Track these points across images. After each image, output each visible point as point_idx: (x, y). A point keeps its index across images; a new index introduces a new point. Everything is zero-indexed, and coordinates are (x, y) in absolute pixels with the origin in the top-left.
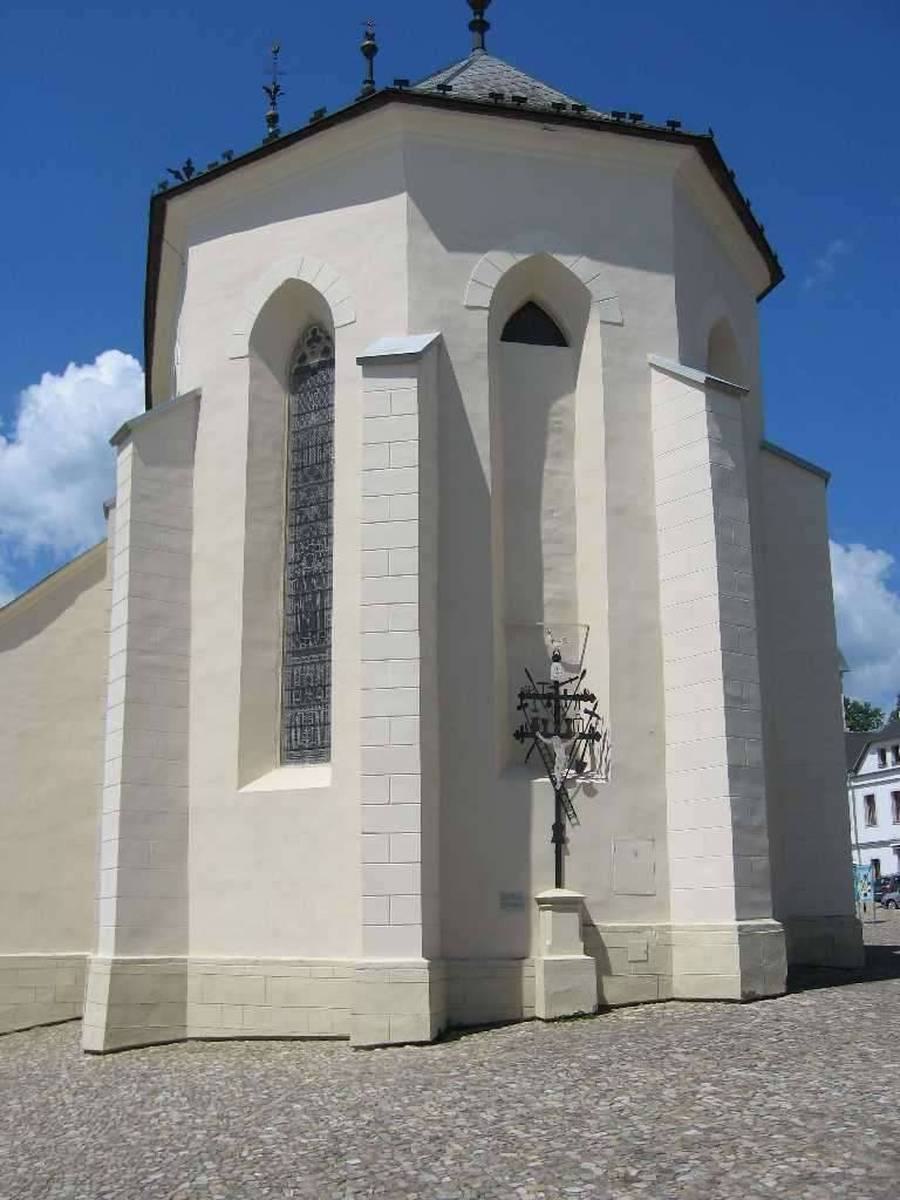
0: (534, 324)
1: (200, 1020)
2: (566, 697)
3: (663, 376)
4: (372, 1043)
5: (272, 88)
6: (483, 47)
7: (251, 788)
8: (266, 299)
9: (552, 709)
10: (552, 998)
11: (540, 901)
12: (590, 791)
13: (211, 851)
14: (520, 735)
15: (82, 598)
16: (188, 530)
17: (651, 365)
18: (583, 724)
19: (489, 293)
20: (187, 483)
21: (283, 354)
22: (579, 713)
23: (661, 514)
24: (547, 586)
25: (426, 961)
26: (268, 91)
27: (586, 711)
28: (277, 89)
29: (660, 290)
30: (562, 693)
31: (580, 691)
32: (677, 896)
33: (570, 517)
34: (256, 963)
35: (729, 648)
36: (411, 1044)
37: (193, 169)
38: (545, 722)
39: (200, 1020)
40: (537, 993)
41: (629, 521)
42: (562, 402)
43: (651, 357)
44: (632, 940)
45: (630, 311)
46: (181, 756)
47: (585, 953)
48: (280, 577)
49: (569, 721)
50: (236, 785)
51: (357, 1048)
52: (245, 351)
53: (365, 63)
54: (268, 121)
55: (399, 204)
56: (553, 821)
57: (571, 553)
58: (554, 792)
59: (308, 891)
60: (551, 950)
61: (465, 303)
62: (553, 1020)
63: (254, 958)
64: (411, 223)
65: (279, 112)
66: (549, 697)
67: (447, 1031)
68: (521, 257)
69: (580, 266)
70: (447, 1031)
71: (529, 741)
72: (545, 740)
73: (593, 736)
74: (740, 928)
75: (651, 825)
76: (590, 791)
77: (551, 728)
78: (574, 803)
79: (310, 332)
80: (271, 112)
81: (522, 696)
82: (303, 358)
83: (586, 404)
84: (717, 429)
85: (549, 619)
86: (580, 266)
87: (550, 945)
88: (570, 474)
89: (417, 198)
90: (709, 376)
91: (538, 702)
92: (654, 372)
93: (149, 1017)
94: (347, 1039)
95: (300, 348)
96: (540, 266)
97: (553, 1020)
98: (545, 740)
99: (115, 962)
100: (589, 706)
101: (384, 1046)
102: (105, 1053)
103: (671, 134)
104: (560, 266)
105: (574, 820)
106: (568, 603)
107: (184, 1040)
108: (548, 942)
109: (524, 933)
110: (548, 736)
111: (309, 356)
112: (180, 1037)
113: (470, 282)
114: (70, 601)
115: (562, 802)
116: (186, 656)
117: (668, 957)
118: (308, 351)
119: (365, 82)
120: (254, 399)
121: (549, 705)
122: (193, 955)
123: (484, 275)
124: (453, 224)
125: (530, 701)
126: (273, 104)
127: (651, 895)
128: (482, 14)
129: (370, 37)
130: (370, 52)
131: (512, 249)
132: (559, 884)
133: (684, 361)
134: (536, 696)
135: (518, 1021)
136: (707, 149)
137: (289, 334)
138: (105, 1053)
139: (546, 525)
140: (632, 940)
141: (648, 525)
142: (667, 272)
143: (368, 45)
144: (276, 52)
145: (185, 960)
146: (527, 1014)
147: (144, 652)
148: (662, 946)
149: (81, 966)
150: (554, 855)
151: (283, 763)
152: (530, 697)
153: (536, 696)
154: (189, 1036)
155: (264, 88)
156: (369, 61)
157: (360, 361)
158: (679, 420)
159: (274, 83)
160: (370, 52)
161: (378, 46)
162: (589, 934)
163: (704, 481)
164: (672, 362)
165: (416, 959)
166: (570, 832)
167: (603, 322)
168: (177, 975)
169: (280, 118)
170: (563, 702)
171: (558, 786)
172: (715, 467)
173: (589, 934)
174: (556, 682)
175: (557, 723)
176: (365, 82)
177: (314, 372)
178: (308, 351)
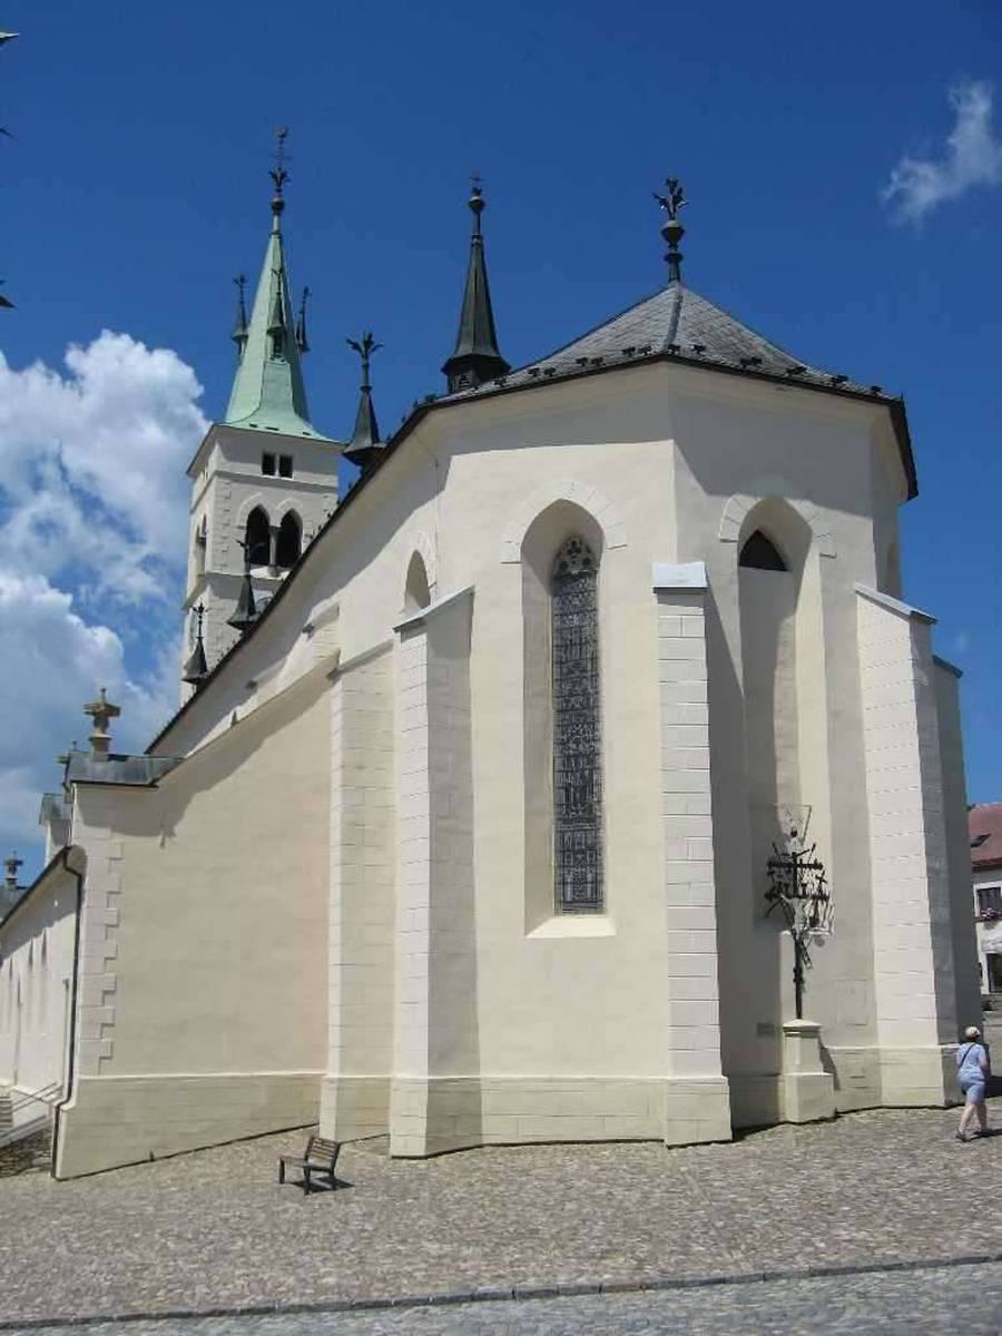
0: (764, 553)
1: (495, 1129)
2: (803, 866)
3: (867, 603)
4: (686, 1142)
5: (279, 176)
6: (679, 279)
7: (535, 934)
8: (536, 514)
9: (791, 876)
10: (805, 1105)
11: (787, 1029)
12: (820, 942)
13: (496, 988)
14: (769, 896)
15: (268, 742)
16: (467, 712)
17: (857, 592)
18: (812, 889)
19: (737, 529)
20: (466, 670)
21: (546, 557)
22: (808, 877)
23: (868, 720)
24: (778, 774)
25: (726, 1078)
26: (274, 176)
27: (817, 877)
28: (283, 176)
29: (863, 528)
30: (798, 862)
31: (812, 862)
32: (883, 1028)
33: (793, 717)
34: (550, 1080)
35: (929, 830)
36: (716, 1142)
37: (372, 343)
38: (787, 886)
39: (495, 1129)
40: (790, 1103)
41: (844, 724)
42: (788, 621)
43: (857, 586)
44: (852, 1061)
45: (837, 544)
46: (470, 906)
47: (825, 1071)
48: (550, 751)
49: (804, 885)
50: (523, 931)
51: (670, 1148)
52: (518, 557)
53: (471, 215)
54: (273, 208)
55: (668, 447)
56: (794, 965)
57: (794, 746)
58: (793, 941)
59: (607, 1017)
60: (800, 1068)
61: (720, 536)
62: (804, 1124)
63: (547, 1076)
64: (677, 465)
65: (285, 199)
66: (789, 865)
67: (740, 1132)
68: (759, 500)
69: (803, 508)
70: (740, 1132)
71: (775, 901)
72: (787, 900)
73: (823, 897)
74: (943, 1051)
75: (861, 968)
76: (820, 942)
77: (791, 891)
78: (809, 951)
79: (569, 543)
80: (276, 200)
81: (771, 864)
82: (564, 565)
83: (806, 624)
84: (917, 653)
85: (781, 801)
86: (803, 508)
87: (796, 1065)
88: (793, 679)
89: (677, 443)
90: (916, 610)
91: (782, 870)
92: (859, 597)
93: (455, 1126)
94: (662, 1141)
95: (567, 559)
96: (772, 506)
97: (804, 1124)
98: (787, 900)
99: (431, 1081)
100: (819, 873)
101: (693, 1145)
102: (426, 1157)
103: (873, 397)
104: (792, 510)
105: (809, 965)
106: (794, 787)
107: (480, 1146)
108: (798, 1062)
109: (776, 1055)
110: (789, 897)
111: (571, 565)
112: (478, 1143)
113: (722, 520)
114: (257, 746)
115: (800, 951)
116: (470, 820)
117: (878, 1073)
118: (567, 559)
119: (474, 237)
120: (526, 599)
121: (789, 872)
122: (486, 1074)
123: (732, 515)
124: (712, 471)
125: (775, 869)
126: (279, 191)
127: (863, 1026)
128: (676, 246)
129: (478, 192)
130: (478, 207)
131: (750, 493)
132: (799, 1016)
133: (880, 589)
134: (781, 865)
135: (772, 1126)
136: (897, 410)
137: (554, 541)
138: (426, 1157)
139: (778, 723)
140: (852, 1061)
141: (856, 725)
142: (865, 515)
143: (476, 201)
144: (283, 136)
145: (479, 1079)
146: (782, 1120)
147: (443, 818)
148: (875, 1063)
149: (311, 1083)
150: (795, 993)
151: (557, 913)
152: (776, 865)
153: (781, 865)
154: (485, 1142)
155: (270, 173)
156: (477, 217)
157: (657, 590)
158: (884, 644)
159: (280, 169)
160: (478, 207)
161: (485, 200)
162: (825, 1056)
163: (909, 693)
164: (872, 590)
165: (718, 1076)
166: (805, 975)
167: (822, 555)
168: (472, 1092)
169: (286, 207)
170: (799, 869)
171: (797, 937)
172: (917, 683)
173: (825, 1056)
174: (794, 853)
175: (796, 889)
176: (474, 237)
177: (575, 578)
178: (567, 559)
